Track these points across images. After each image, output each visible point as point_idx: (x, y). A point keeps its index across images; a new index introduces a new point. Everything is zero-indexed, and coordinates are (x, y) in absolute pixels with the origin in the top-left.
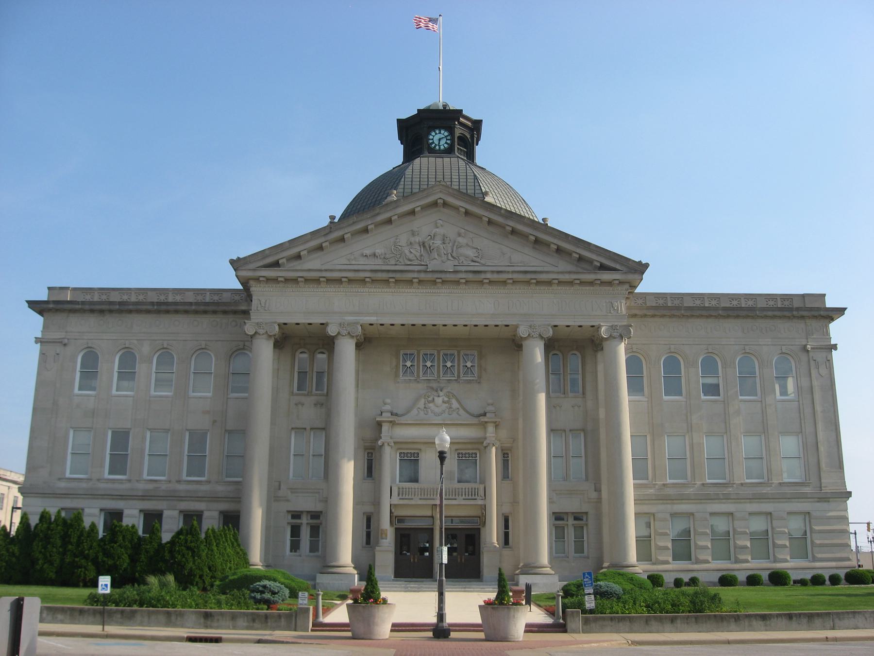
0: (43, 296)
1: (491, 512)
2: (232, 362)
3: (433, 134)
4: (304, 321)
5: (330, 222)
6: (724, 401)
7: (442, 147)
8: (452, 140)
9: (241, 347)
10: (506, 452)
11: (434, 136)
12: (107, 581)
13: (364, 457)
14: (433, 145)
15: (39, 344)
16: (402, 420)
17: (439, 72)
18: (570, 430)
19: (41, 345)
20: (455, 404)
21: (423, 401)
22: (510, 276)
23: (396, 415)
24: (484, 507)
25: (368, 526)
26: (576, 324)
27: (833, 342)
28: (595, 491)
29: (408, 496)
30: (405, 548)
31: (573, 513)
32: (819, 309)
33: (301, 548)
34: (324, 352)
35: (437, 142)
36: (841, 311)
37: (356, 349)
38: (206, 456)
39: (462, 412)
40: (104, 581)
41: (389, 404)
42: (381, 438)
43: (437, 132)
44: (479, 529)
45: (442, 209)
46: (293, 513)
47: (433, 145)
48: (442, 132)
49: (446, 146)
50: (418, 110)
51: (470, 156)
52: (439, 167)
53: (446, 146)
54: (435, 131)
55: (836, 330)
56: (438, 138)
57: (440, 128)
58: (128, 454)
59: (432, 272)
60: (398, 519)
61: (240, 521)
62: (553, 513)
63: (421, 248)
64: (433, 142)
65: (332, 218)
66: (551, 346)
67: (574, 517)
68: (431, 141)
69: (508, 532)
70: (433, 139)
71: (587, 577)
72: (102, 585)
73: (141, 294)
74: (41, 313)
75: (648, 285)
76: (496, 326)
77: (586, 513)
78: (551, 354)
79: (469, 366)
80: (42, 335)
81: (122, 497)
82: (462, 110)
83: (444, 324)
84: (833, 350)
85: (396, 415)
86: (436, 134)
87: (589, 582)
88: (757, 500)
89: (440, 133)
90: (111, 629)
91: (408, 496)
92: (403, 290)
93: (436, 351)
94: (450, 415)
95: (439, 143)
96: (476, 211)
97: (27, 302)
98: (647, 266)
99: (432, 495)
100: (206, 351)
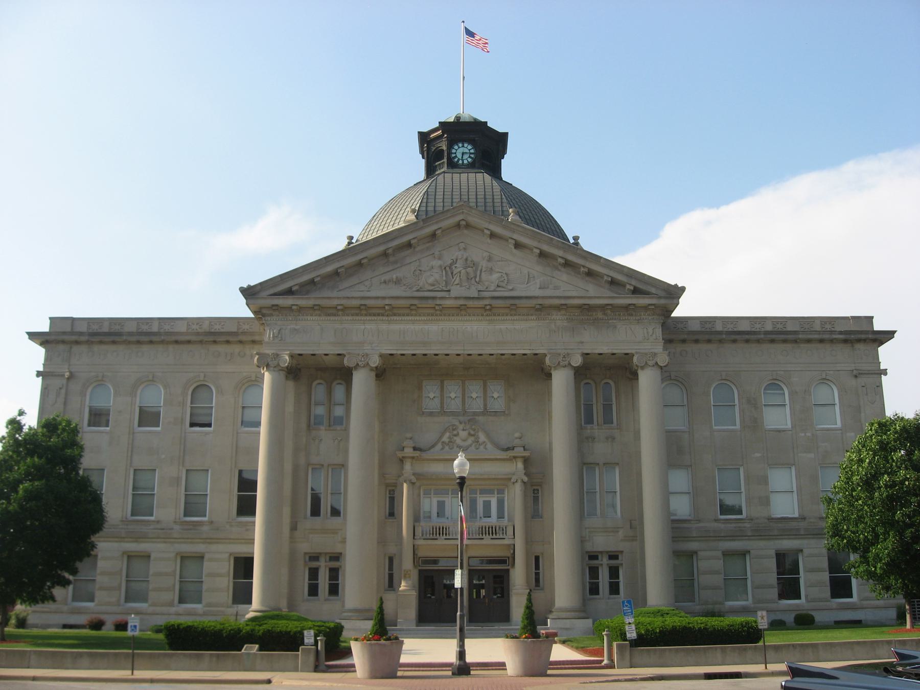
0: (45, 327)
3: (456, 147)
4: (606, 351)
5: (348, 243)
6: (689, 432)
7: (465, 162)
8: (449, 153)
9: (151, 378)
10: (536, 488)
11: (456, 150)
12: (136, 622)
13: (386, 494)
14: (456, 160)
15: (41, 377)
16: (425, 455)
17: (465, 76)
19: (42, 379)
20: (482, 437)
21: (447, 434)
22: (387, 302)
23: (420, 450)
24: (512, 547)
25: (391, 567)
26: (465, 353)
27: (882, 367)
29: (492, 535)
31: (607, 552)
32: (866, 332)
33: (860, 619)
34: (589, 382)
35: (459, 156)
36: (889, 335)
37: (376, 380)
38: (207, 495)
39: (489, 446)
40: (133, 622)
41: (517, 438)
42: (403, 475)
43: (460, 145)
44: (508, 571)
45: (466, 231)
46: (331, 555)
47: (456, 160)
48: (466, 145)
49: (470, 160)
50: (439, 122)
51: (495, 171)
52: (472, 181)
53: (470, 160)
54: (457, 145)
55: (885, 353)
56: (463, 152)
57: (463, 141)
58: (154, 494)
59: (456, 298)
61: (510, 574)
63: (442, 272)
64: (459, 159)
65: (351, 238)
66: (380, 374)
67: (609, 556)
68: (453, 155)
70: (455, 153)
71: (626, 606)
72: (131, 626)
73: (218, 323)
74: (42, 344)
75: (681, 311)
76: (458, 355)
77: (622, 552)
78: (582, 383)
79: (453, 397)
80: (44, 368)
82: (487, 122)
83: (326, 353)
84: (882, 375)
85: (420, 450)
86: (459, 147)
87: (629, 611)
88: (786, 537)
89: (463, 146)
90: (139, 674)
91: (492, 535)
92: (306, 317)
94: (451, 449)
95: (462, 157)
97: (28, 333)
98: (683, 289)
99: (435, 535)
100: (256, 383)
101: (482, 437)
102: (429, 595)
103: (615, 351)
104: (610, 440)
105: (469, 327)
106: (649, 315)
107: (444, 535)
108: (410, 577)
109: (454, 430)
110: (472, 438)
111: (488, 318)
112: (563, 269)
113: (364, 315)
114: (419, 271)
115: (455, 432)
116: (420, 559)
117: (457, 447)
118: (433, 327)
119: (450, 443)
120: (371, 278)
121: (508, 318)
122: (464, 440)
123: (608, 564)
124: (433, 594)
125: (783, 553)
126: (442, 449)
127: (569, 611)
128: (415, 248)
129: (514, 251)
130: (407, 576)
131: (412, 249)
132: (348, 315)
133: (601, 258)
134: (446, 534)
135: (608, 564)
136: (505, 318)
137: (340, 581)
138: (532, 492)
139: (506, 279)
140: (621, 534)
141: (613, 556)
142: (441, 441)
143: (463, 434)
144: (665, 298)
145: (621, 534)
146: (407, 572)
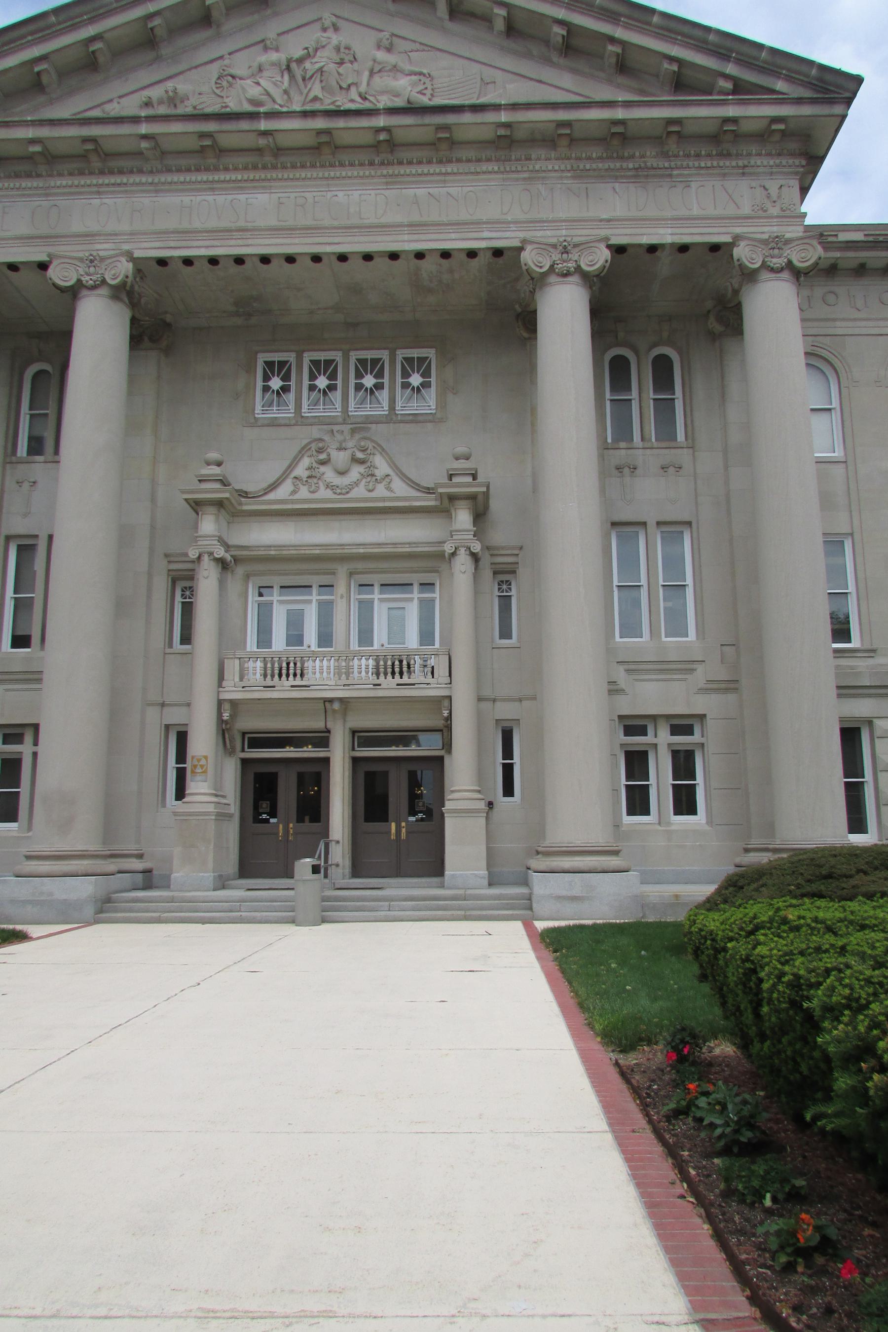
1: (292, 595)
2: (8, 472)
18: (658, 523)
21: (306, 461)
28: (722, 662)
30: (264, 806)
60: (359, 737)
62: (621, 717)
69: (511, 765)
77: (702, 717)
81: (707, 737)
93: (340, 354)
94: (370, 491)
96: (509, 892)
101: (382, 466)
102: (264, 816)
103: (687, 240)
104: (671, 470)
105: (340, 194)
106: (769, 155)
107: (291, 676)
108: (205, 772)
109: (320, 451)
110: (361, 469)
111: (385, 172)
112: (562, 61)
113: (97, 171)
114: (230, 79)
115: (323, 456)
116: (247, 736)
117: (327, 487)
118: (256, 196)
119: (309, 480)
120: (120, 97)
121: (432, 169)
122: (342, 473)
123: (669, 745)
124: (273, 814)
125: (687, 751)
126: (294, 492)
127: (622, 407)
128: (219, 26)
129: (449, 25)
130: (199, 770)
131: (214, 27)
132: (60, 175)
133: (652, 11)
134: (295, 675)
135: (669, 745)
136: (425, 169)
137: (24, 790)
138: (496, 587)
139: (430, 87)
140: (700, 676)
141: (681, 727)
142: (293, 475)
143: (340, 458)
144: (813, 101)
145: (700, 676)
146: (199, 760)
